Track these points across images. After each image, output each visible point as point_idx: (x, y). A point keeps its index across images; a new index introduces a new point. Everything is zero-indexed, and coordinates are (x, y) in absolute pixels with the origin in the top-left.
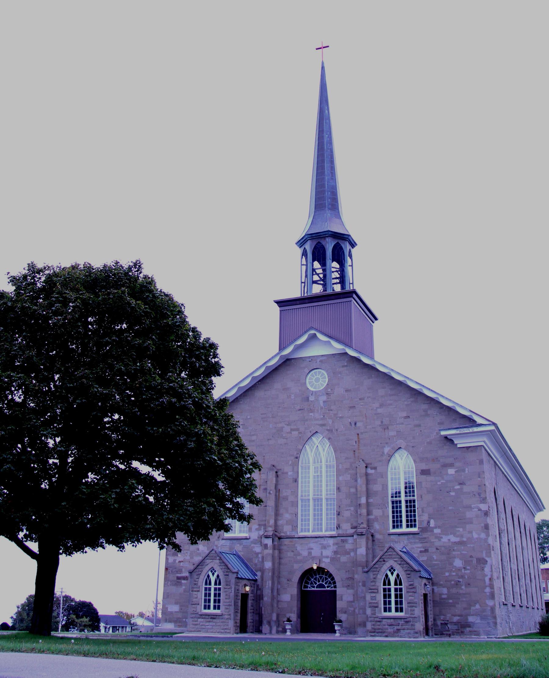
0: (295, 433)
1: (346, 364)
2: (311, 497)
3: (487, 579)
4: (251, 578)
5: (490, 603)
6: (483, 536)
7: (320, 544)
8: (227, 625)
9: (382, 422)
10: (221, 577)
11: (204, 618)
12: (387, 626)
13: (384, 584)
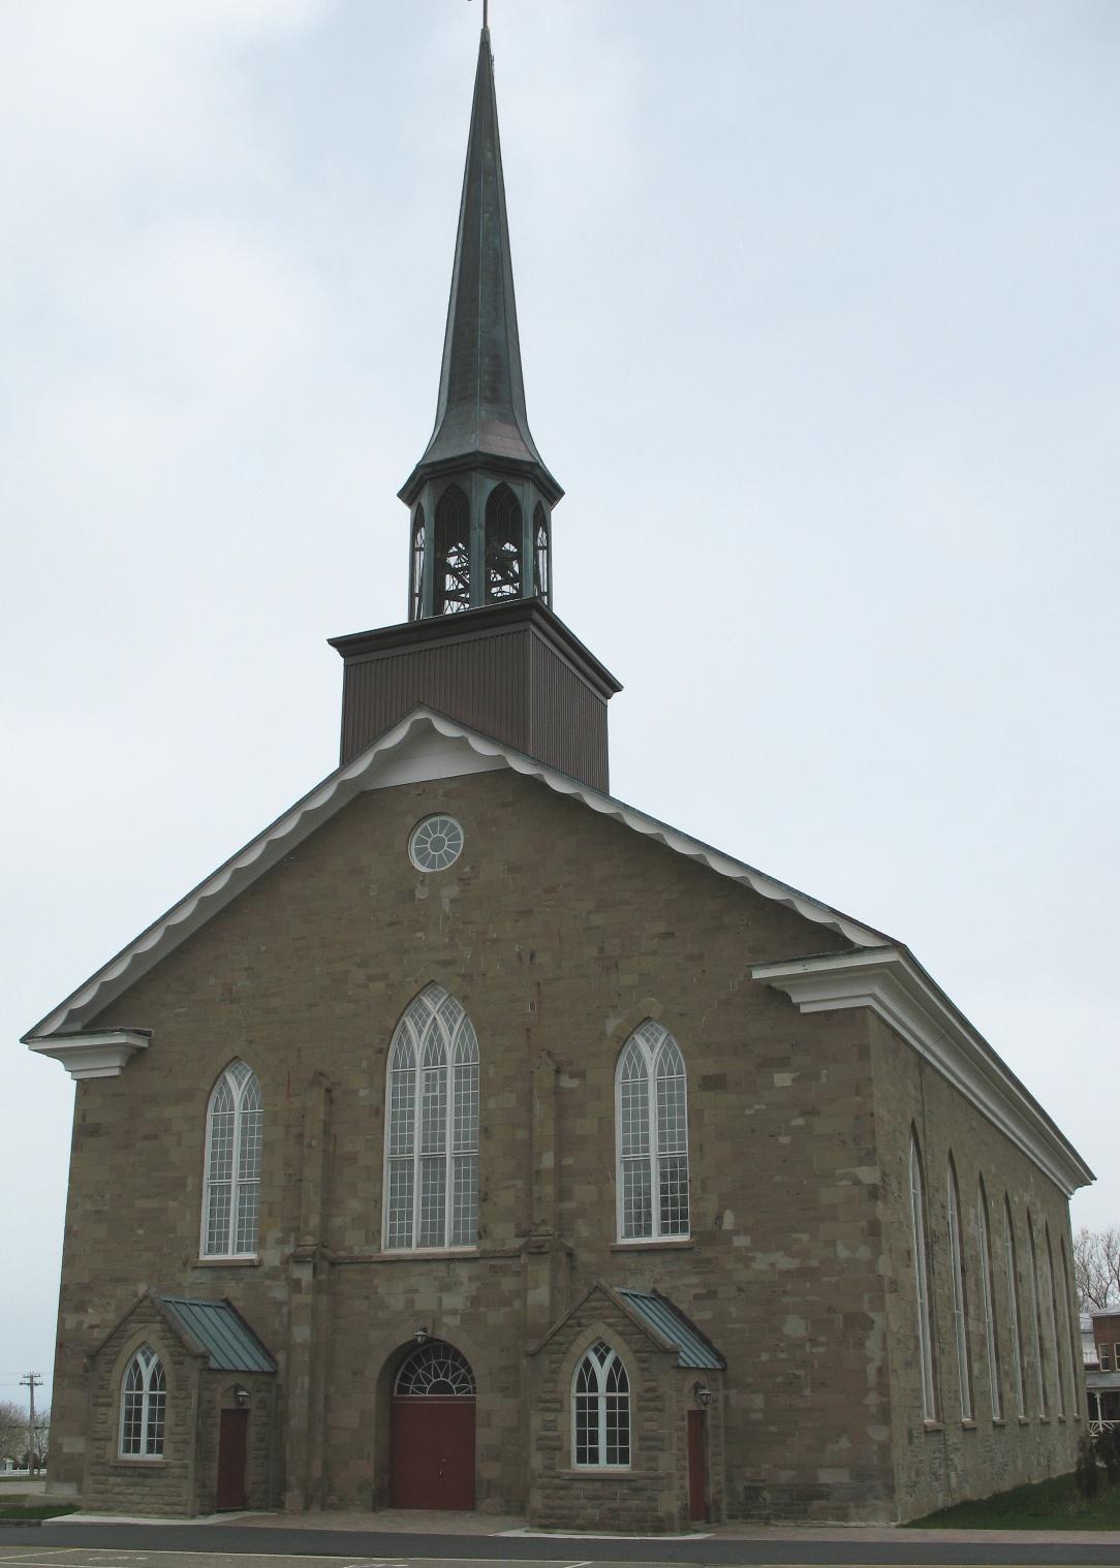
0: (378, 987)
1: (511, 798)
2: (416, 1155)
3: (872, 1371)
4: (254, 1368)
5: (878, 1434)
6: (864, 1253)
7: (436, 1278)
8: (179, 1495)
9: (601, 950)
10: (167, 1368)
11: (124, 1475)
12: (583, 1501)
13: (581, 1388)
